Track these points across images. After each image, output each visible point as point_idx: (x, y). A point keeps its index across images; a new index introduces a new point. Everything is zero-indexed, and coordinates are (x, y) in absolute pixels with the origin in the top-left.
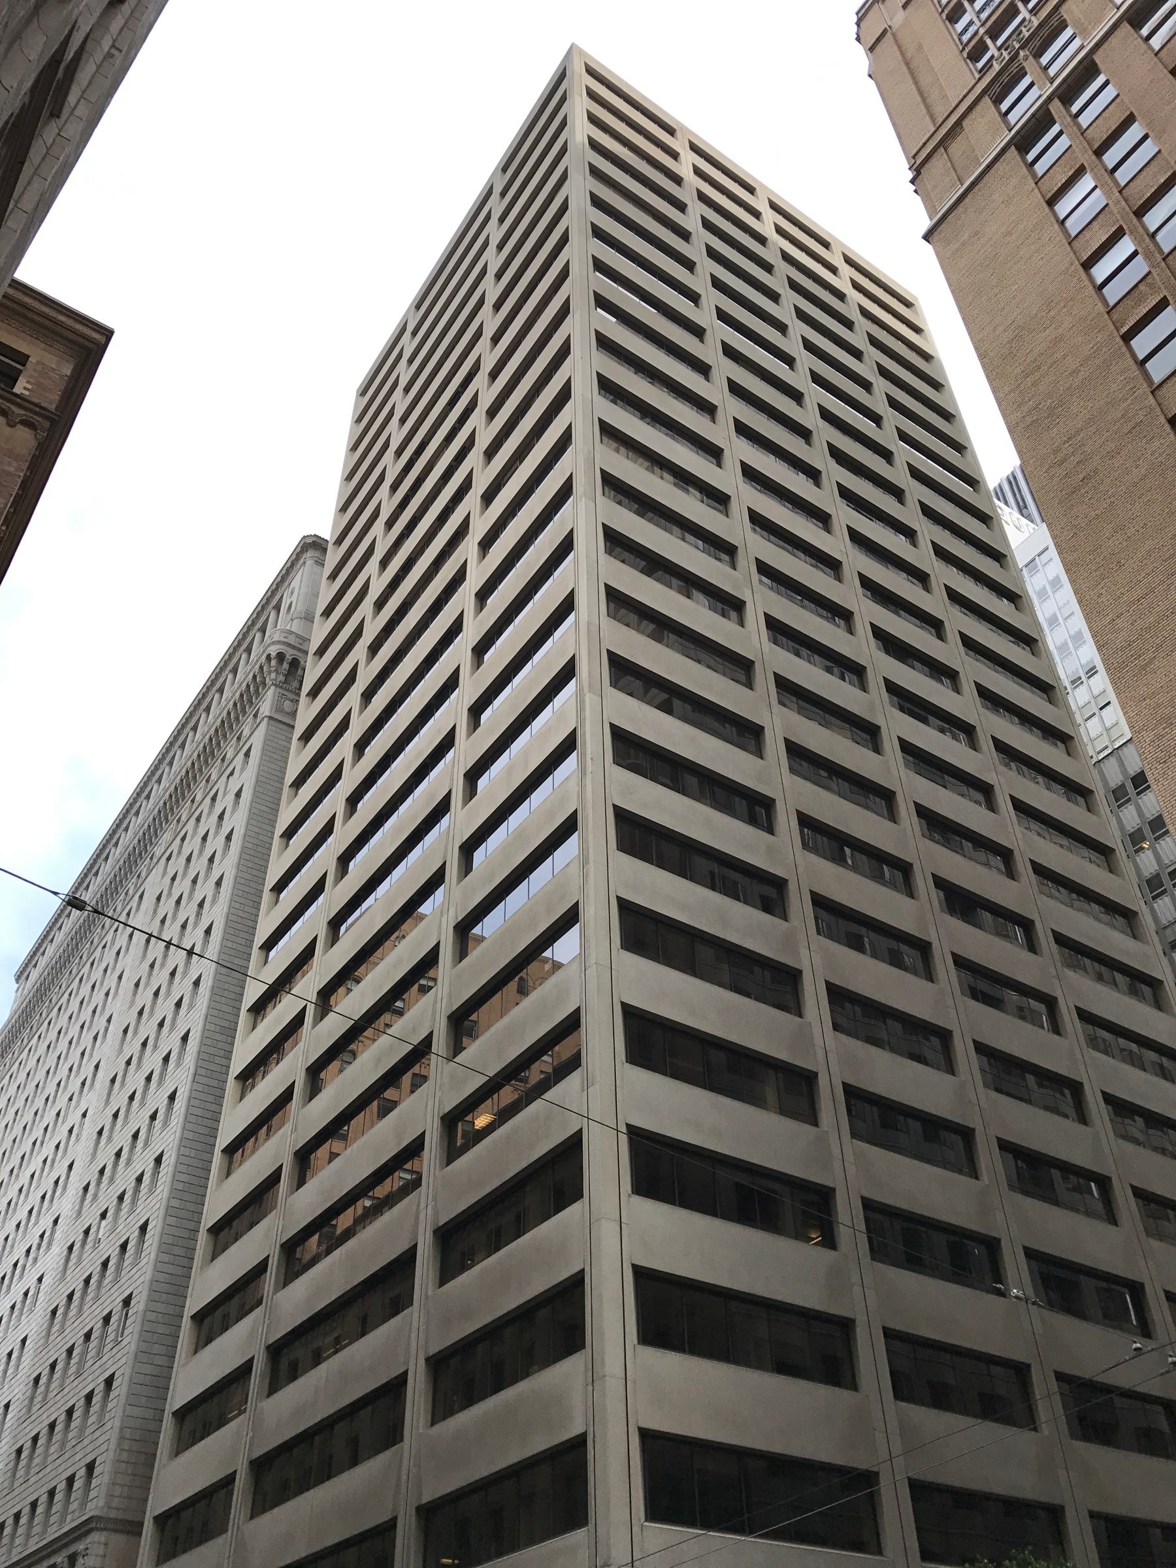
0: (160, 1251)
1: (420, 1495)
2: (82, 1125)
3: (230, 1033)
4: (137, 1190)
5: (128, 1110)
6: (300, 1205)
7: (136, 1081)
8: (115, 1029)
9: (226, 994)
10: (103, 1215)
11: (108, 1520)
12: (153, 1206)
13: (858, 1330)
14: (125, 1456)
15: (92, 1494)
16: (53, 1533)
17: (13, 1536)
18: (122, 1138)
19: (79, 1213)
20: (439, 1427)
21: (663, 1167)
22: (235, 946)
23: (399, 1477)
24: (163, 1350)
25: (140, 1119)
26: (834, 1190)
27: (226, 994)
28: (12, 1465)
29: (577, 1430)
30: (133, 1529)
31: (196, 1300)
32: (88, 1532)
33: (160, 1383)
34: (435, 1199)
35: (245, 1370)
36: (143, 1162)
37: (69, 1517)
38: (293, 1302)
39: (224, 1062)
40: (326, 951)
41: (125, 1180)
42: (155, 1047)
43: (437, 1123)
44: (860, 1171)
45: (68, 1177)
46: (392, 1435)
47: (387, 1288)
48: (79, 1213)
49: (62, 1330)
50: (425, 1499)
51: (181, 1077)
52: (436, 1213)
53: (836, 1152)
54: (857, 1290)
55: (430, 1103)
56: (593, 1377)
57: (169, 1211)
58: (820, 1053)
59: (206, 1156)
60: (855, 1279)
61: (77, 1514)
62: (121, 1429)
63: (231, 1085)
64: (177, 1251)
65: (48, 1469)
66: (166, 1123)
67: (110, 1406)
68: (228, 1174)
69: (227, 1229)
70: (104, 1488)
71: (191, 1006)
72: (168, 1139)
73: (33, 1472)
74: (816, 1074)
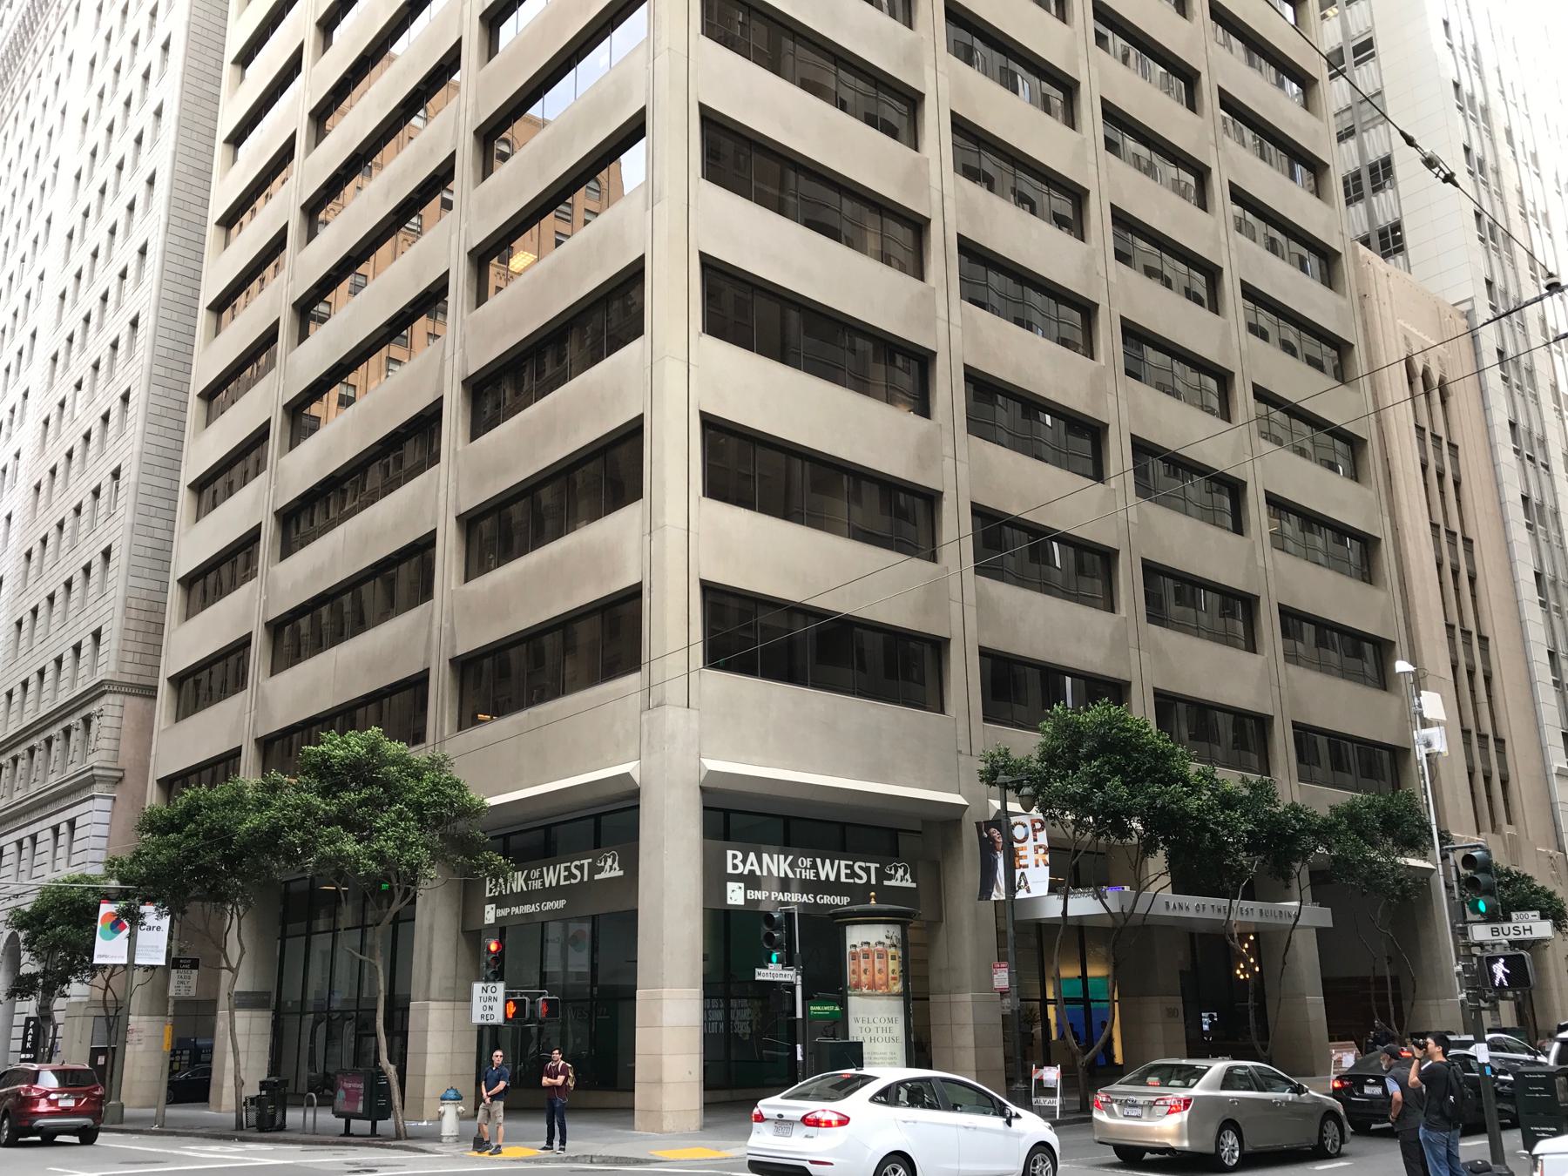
0: (147, 421)
1: (454, 647)
2: (40, 289)
3: (206, 175)
4: (113, 358)
5: (92, 270)
6: (302, 362)
7: (97, 234)
8: (66, 175)
9: (198, 128)
10: (78, 386)
11: (122, 684)
12: (134, 372)
13: (945, 503)
14: (132, 625)
15: (101, 660)
16: (63, 698)
17: (23, 703)
18: (90, 301)
19: (51, 384)
20: (475, 584)
21: (741, 307)
22: (201, 67)
23: (430, 633)
24: (163, 524)
25: (107, 278)
26: (934, 354)
27: (198, 128)
28: (13, 637)
29: (633, 581)
30: (150, 692)
31: (193, 468)
32: (104, 693)
33: (163, 554)
34: (463, 347)
35: (253, 537)
36: (117, 326)
37: (79, 683)
38: (298, 468)
39: (201, 211)
40: (316, 61)
41: (98, 347)
42: (116, 193)
43: (464, 258)
44: (964, 336)
45: (32, 348)
46: (424, 591)
47: (414, 442)
48: (51, 384)
49: (49, 505)
50: (461, 650)
51: (152, 226)
52: (465, 361)
53: (942, 313)
54: (949, 463)
55: (454, 238)
56: (651, 528)
57: (153, 379)
58: (936, 196)
59: (189, 320)
60: (948, 450)
61: (87, 679)
62: (126, 599)
63: (212, 231)
64: (166, 422)
65: (52, 639)
66: (139, 280)
67: (110, 576)
68: (217, 332)
69: (217, 393)
70: (113, 655)
71: (155, 141)
72: (143, 298)
73: (36, 642)
74: (928, 221)
